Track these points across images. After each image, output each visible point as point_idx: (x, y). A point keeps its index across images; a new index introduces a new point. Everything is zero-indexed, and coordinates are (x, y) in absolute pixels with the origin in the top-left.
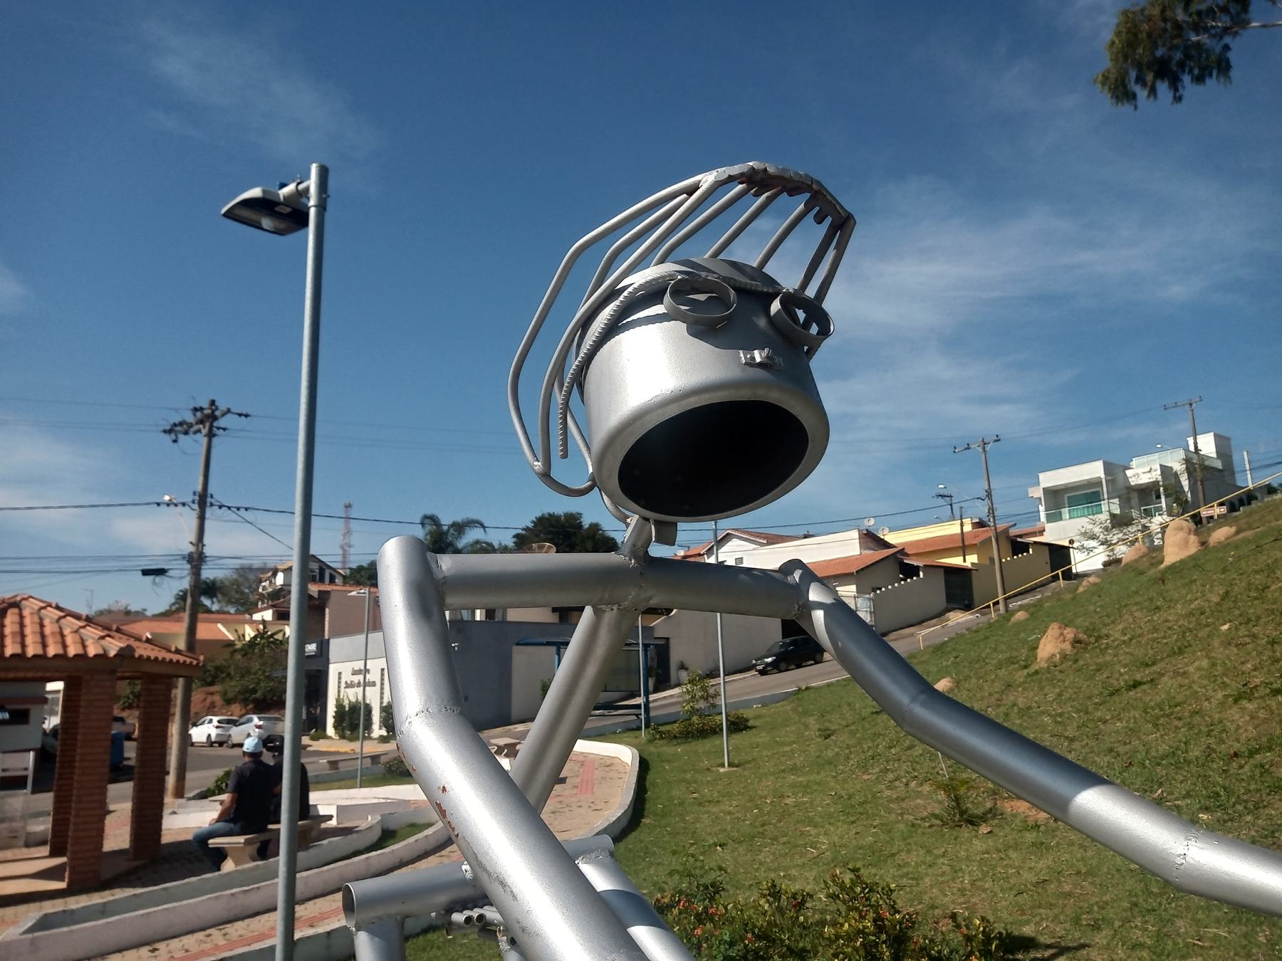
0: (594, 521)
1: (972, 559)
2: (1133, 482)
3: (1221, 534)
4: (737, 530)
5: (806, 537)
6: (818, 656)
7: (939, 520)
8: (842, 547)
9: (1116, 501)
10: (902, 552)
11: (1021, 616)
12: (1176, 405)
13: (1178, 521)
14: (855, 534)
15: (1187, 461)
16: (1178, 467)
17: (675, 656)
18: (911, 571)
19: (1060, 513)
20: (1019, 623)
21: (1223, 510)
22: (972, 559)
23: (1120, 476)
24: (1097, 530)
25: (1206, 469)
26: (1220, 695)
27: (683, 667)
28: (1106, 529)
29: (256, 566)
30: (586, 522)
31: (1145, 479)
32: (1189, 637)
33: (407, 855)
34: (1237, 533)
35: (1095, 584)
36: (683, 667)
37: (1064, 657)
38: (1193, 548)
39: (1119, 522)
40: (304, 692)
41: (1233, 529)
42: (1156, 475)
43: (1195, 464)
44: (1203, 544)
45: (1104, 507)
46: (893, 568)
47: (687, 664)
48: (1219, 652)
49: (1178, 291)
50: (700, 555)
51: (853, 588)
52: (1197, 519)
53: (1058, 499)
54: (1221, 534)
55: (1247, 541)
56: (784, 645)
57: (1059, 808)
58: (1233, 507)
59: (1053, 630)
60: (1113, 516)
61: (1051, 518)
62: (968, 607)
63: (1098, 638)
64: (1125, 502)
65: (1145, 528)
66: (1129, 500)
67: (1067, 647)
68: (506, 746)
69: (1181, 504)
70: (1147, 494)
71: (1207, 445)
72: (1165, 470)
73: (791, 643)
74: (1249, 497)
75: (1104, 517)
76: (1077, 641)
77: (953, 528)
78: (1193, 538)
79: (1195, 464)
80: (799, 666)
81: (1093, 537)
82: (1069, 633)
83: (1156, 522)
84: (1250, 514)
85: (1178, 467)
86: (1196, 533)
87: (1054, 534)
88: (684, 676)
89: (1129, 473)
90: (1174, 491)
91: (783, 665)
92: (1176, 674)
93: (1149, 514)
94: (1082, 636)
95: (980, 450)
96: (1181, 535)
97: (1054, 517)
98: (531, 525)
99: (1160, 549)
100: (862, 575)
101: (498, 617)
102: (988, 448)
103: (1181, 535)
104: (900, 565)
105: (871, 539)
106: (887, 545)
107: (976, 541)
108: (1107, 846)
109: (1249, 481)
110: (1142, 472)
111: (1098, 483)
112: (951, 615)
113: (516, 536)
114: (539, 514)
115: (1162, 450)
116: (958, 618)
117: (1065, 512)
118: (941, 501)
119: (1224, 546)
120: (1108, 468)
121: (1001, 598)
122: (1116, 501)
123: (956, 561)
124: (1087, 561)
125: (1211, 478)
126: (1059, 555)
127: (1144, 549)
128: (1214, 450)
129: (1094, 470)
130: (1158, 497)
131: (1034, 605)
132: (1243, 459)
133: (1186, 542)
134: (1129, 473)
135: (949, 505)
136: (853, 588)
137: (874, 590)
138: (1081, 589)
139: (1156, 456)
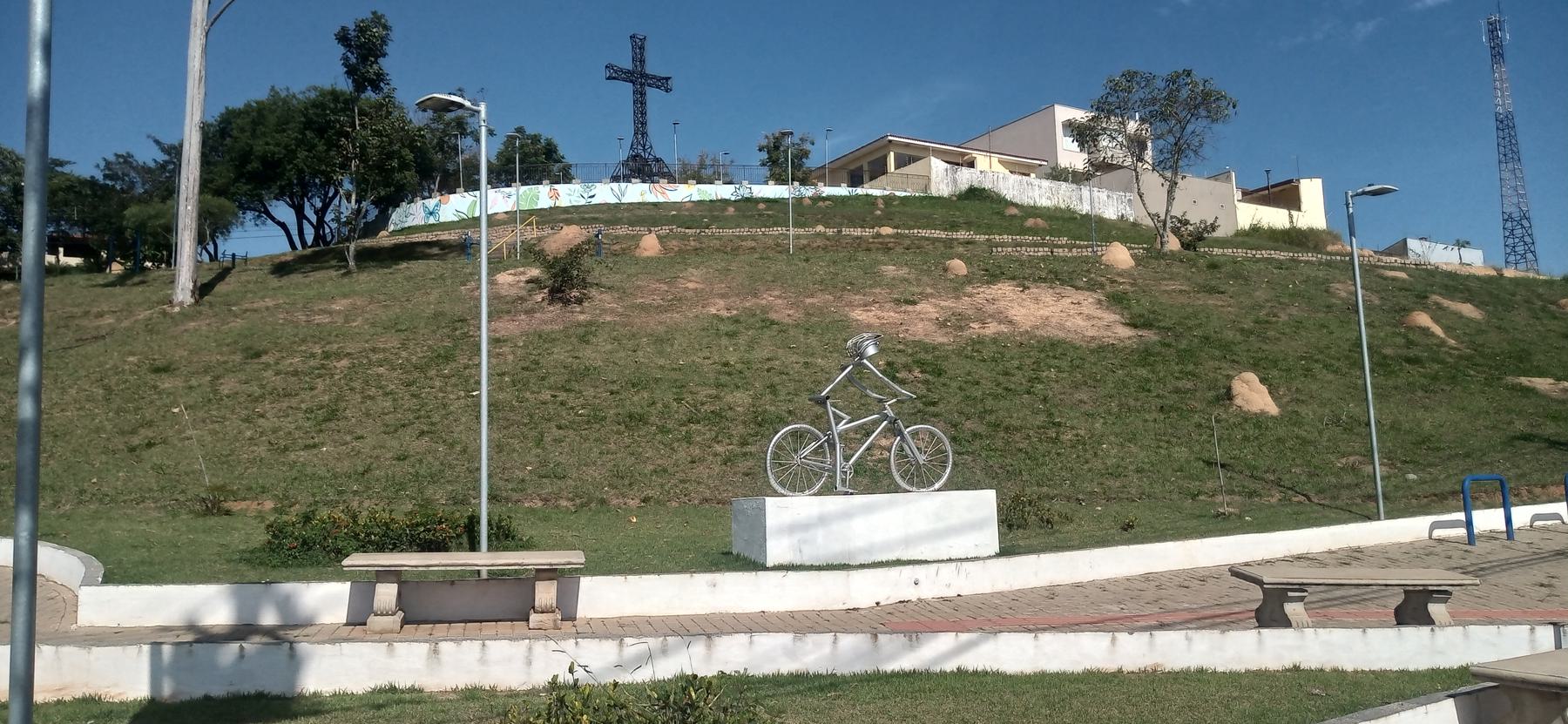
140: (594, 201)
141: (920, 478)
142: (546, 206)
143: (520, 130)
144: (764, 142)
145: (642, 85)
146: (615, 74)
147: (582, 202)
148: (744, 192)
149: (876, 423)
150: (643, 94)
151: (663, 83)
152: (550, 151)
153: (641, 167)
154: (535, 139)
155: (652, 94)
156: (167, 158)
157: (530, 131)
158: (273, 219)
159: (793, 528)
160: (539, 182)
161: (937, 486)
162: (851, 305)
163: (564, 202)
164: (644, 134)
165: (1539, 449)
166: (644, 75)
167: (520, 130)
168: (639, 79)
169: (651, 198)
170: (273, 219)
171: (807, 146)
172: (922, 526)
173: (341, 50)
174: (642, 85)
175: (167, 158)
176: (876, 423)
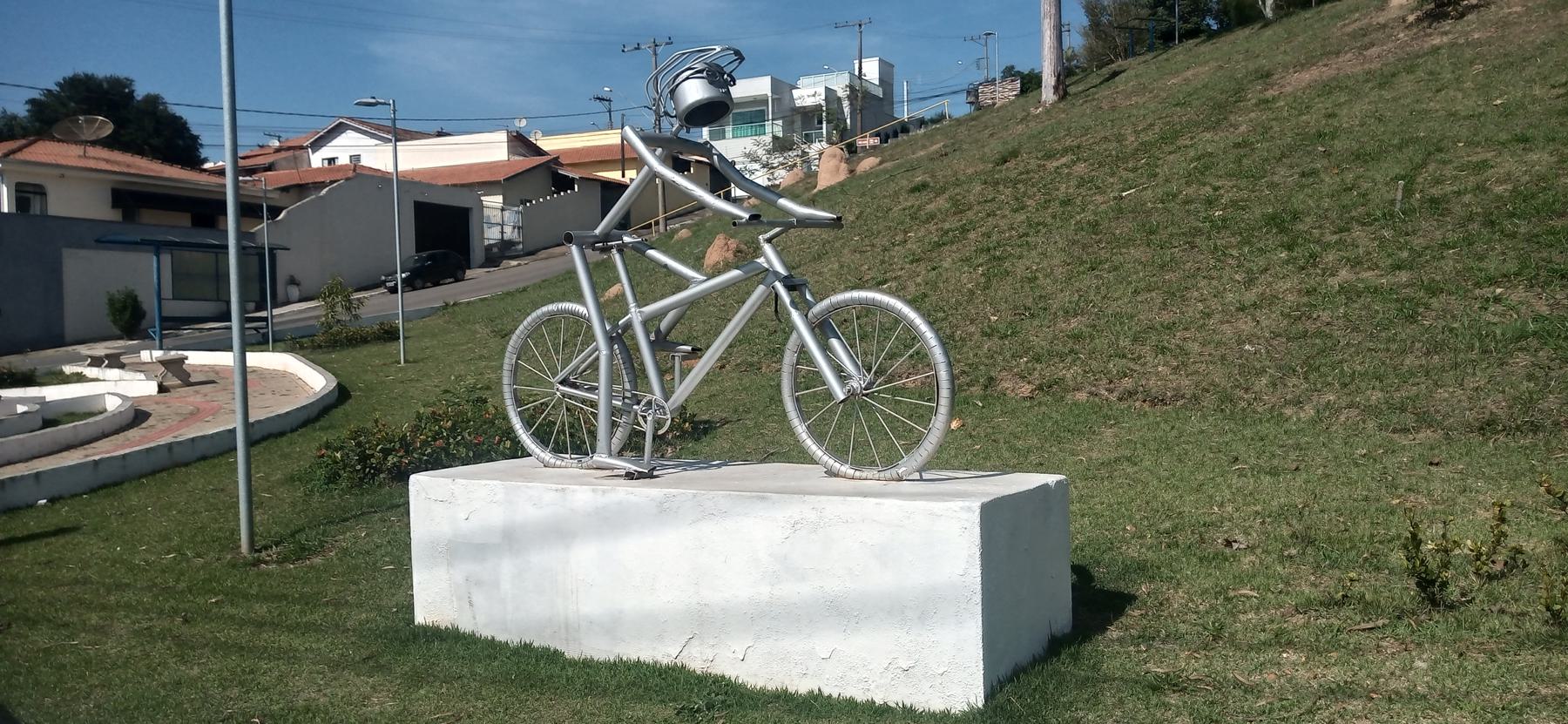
0: (154, 91)
2: (799, 103)
3: (868, 163)
4: (352, 119)
5: (440, 134)
6: (459, 273)
7: (595, 127)
8: (488, 149)
9: (780, 122)
10: (556, 160)
11: (684, 233)
13: (835, 149)
14: (502, 136)
15: (851, 87)
16: (842, 93)
17: (287, 265)
18: (563, 184)
21: (877, 141)
23: (787, 97)
24: (761, 152)
25: (867, 95)
27: (293, 281)
28: (769, 152)
29: (928, 117)
30: (140, 92)
31: (809, 102)
32: (828, 247)
33: (83, 435)
34: (881, 163)
36: (293, 281)
38: (842, 176)
39: (781, 145)
40: (417, 179)
41: (878, 160)
42: (820, 99)
43: (858, 92)
44: (852, 171)
45: (768, 129)
46: (544, 180)
47: (298, 277)
48: (847, 257)
50: (301, 148)
51: (499, 199)
52: (852, 149)
54: (868, 163)
55: (886, 171)
56: (420, 258)
57: (774, 204)
58: (885, 140)
59: (719, 241)
60: (775, 138)
64: (788, 126)
65: (805, 153)
66: (793, 122)
67: (730, 255)
68: (107, 356)
69: (844, 138)
70: (809, 117)
71: (871, 70)
73: (429, 258)
74: (904, 128)
75: (768, 139)
76: (738, 251)
77: (611, 138)
78: (844, 166)
79: (858, 92)
80: (437, 284)
81: (755, 160)
82: (733, 244)
83: (814, 149)
84: (897, 145)
85: (842, 93)
86: (847, 161)
88: (294, 292)
89: (796, 93)
90: (835, 117)
91: (418, 283)
93: (809, 139)
94: (743, 247)
96: (834, 162)
98: (55, 88)
99: (815, 174)
100: (509, 184)
101: (36, 209)
104: (555, 176)
105: (520, 142)
106: (539, 152)
109: (904, 113)
110: (808, 93)
111: (763, 101)
113: (32, 102)
114: (69, 73)
115: (829, 71)
117: (729, 129)
118: (599, 106)
119: (868, 175)
120: (776, 85)
121: (661, 217)
122: (780, 122)
123: (614, 175)
125: (871, 106)
127: (801, 175)
128: (877, 76)
130: (820, 122)
131: (696, 225)
132: (902, 90)
133: (838, 169)
134: (796, 93)
135: (607, 111)
136: (499, 199)
137: (523, 202)
139: (822, 78)
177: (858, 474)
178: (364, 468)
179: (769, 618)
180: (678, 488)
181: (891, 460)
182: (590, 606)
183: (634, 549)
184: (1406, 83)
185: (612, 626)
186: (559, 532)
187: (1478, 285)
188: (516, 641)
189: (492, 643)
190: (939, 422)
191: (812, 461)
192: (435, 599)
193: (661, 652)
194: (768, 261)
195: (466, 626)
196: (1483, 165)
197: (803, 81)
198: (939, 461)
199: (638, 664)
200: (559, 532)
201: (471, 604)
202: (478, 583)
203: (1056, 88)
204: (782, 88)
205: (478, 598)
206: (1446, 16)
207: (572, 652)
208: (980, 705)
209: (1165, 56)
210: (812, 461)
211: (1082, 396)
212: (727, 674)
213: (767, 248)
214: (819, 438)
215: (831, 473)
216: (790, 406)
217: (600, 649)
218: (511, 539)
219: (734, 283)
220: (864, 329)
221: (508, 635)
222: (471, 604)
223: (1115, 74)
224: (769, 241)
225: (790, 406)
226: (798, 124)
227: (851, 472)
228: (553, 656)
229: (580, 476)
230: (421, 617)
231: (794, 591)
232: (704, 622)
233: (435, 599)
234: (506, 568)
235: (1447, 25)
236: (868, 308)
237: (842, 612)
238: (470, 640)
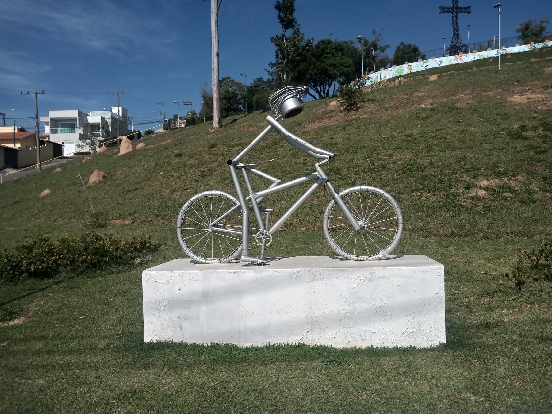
1: (18, 145)
12: (113, 93)
19: (57, 130)
20: (57, 173)
22: (18, 145)
26: (168, 191)
35: (90, 160)
37: (100, 182)
38: (131, 149)
49: (96, 44)
53: (56, 124)
59: (96, 172)
61: (53, 132)
62: (15, 167)
63: (112, 176)
67: (101, 178)
72: (103, 119)
76: (104, 177)
78: (131, 146)
82: (102, 174)
87: (55, 138)
92: (149, 186)
94: (106, 175)
95: (34, 96)
96: (127, 144)
97: (54, 131)
102: (38, 95)
103: (127, 144)
107: (21, 137)
108: (292, 187)
110: (94, 118)
111: (75, 119)
112: (7, 170)
116: (11, 172)
117: (59, 130)
119: (140, 150)
120: (80, 113)
122: (82, 128)
123: (11, 145)
124: (69, 150)
126: (58, 149)
129: (74, 114)
130: (99, 129)
133: (129, 146)
138: (84, 161)
139: (99, 113)
140: (428, 68)
141: (363, 245)
142: (406, 73)
143: (402, 44)
144: (520, 27)
145: (456, 12)
146: (444, 10)
147: (423, 69)
148: (503, 52)
149: (304, 186)
150: (457, 17)
151: (467, 10)
152: (415, 50)
153: (454, 50)
154: (409, 46)
155: (460, 15)
156: (271, 77)
157: (407, 43)
158: (310, 95)
159: (170, 305)
160: (404, 64)
161: (381, 254)
162: (513, 94)
163: (414, 70)
164: (458, 35)
165: (261, 113)
166: (457, 8)
167: (402, 44)
168: (455, 10)
169: (455, 62)
170: (310, 95)
171: (544, 25)
172: (333, 307)
173: (276, 12)
174: (456, 12)
175: (271, 77)
176: (304, 186)
177: (359, 258)
178: (14, 272)
179: (346, 319)
180: (278, 270)
181: (374, 252)
182: (252, 323)
183: (276, 296)
184: (351, 129)
185: (264, 330)
186: (236, 292)
187: (412, 192)
188: (209, 344)
189: (194, 346)
190: (397, 237)
191: (187, 257)
192: (156, 328)
193: (294, 339)
194: (320, 174)
195: (178, 339)
196: (391, 156)
197: (90, 114)
198: (400, 252)
199: (279, 346)
200: (236, 292)
201: (181, 328)
202: (186, 319)
203: (219, 123)
204: (83, 116)
205: (185, 325)
206: (352, 109)
207: (242, 345)
208: (445, 342)
209: (250, 115)
210: (187, 257)
211: (303, 229)
212: (326, 345)
213: (319, 169)
214: (340, 245)
215: (194, 262)
216: (326, 232)
217: (259, 342)
218: (207, 297)
219: (302, 184)
220: (360, 203)
221: (207, 342)
222: (181, 328)
223: (235, 120)
224: (319, 166)
225: (326, 232)
226: (89, 129)
227: (356, 258)
228: (233, 348)
229: (225, 266)
230: (147, 339)
231: (360, 306)
232: (313, 323)
233: (156, 328)
234: (204, 309)
235: (354, 112)
236: (207, 199)
237: (382, 313)
238: (182, 346)
